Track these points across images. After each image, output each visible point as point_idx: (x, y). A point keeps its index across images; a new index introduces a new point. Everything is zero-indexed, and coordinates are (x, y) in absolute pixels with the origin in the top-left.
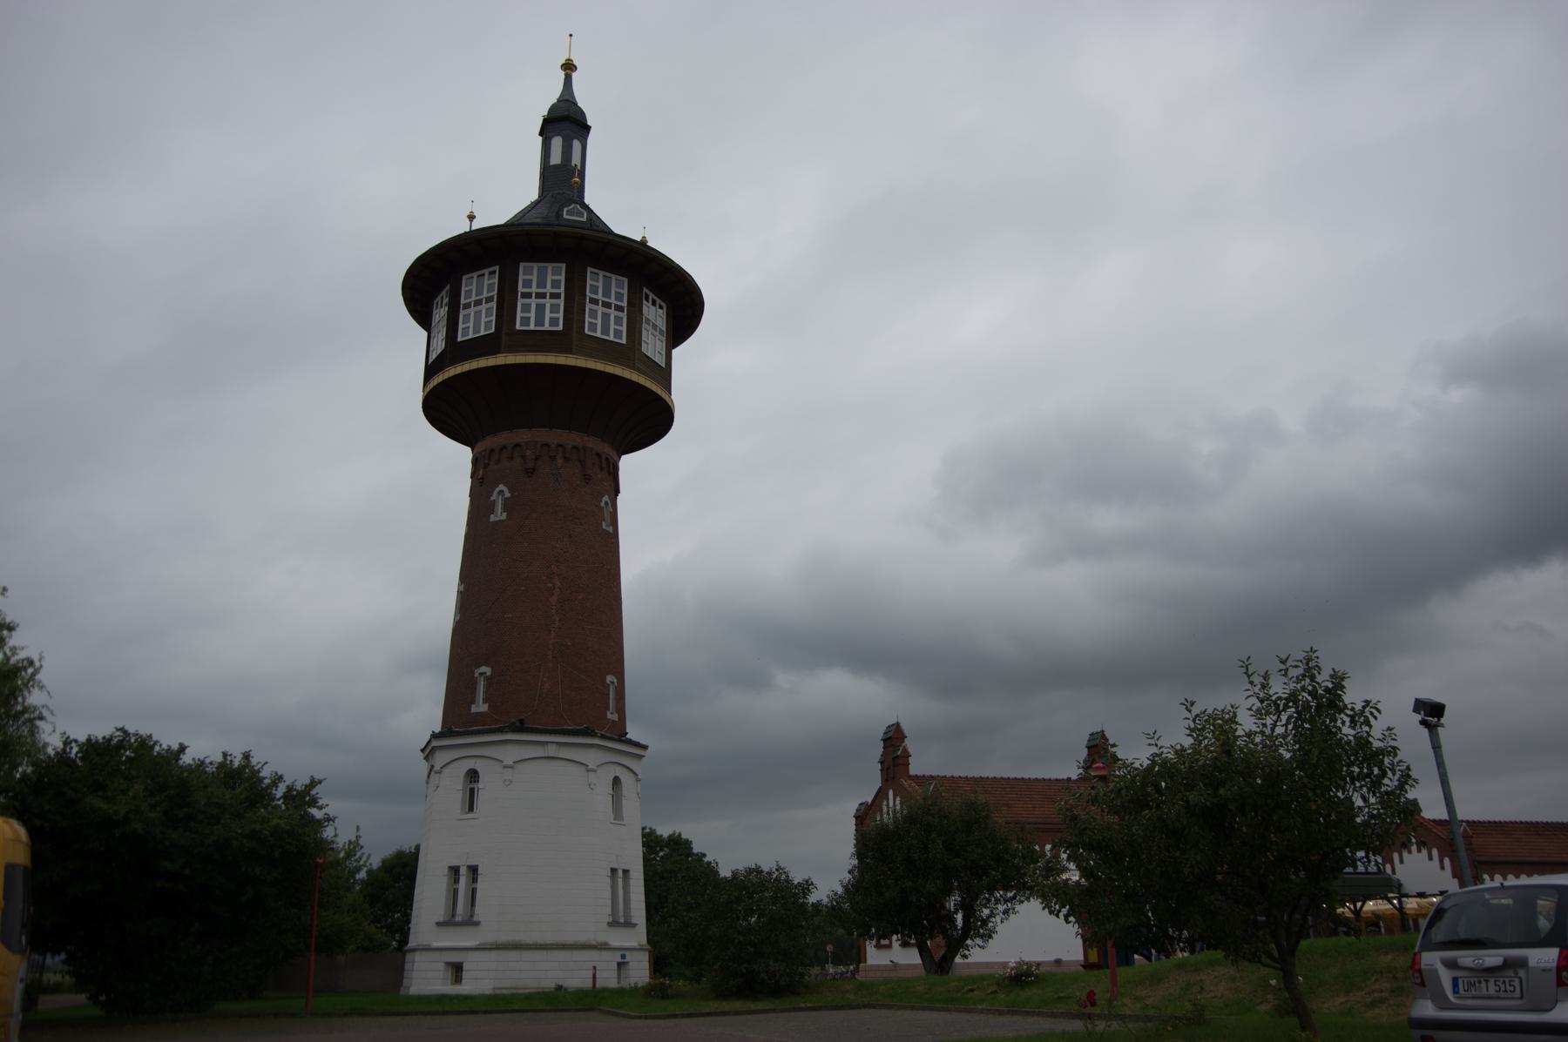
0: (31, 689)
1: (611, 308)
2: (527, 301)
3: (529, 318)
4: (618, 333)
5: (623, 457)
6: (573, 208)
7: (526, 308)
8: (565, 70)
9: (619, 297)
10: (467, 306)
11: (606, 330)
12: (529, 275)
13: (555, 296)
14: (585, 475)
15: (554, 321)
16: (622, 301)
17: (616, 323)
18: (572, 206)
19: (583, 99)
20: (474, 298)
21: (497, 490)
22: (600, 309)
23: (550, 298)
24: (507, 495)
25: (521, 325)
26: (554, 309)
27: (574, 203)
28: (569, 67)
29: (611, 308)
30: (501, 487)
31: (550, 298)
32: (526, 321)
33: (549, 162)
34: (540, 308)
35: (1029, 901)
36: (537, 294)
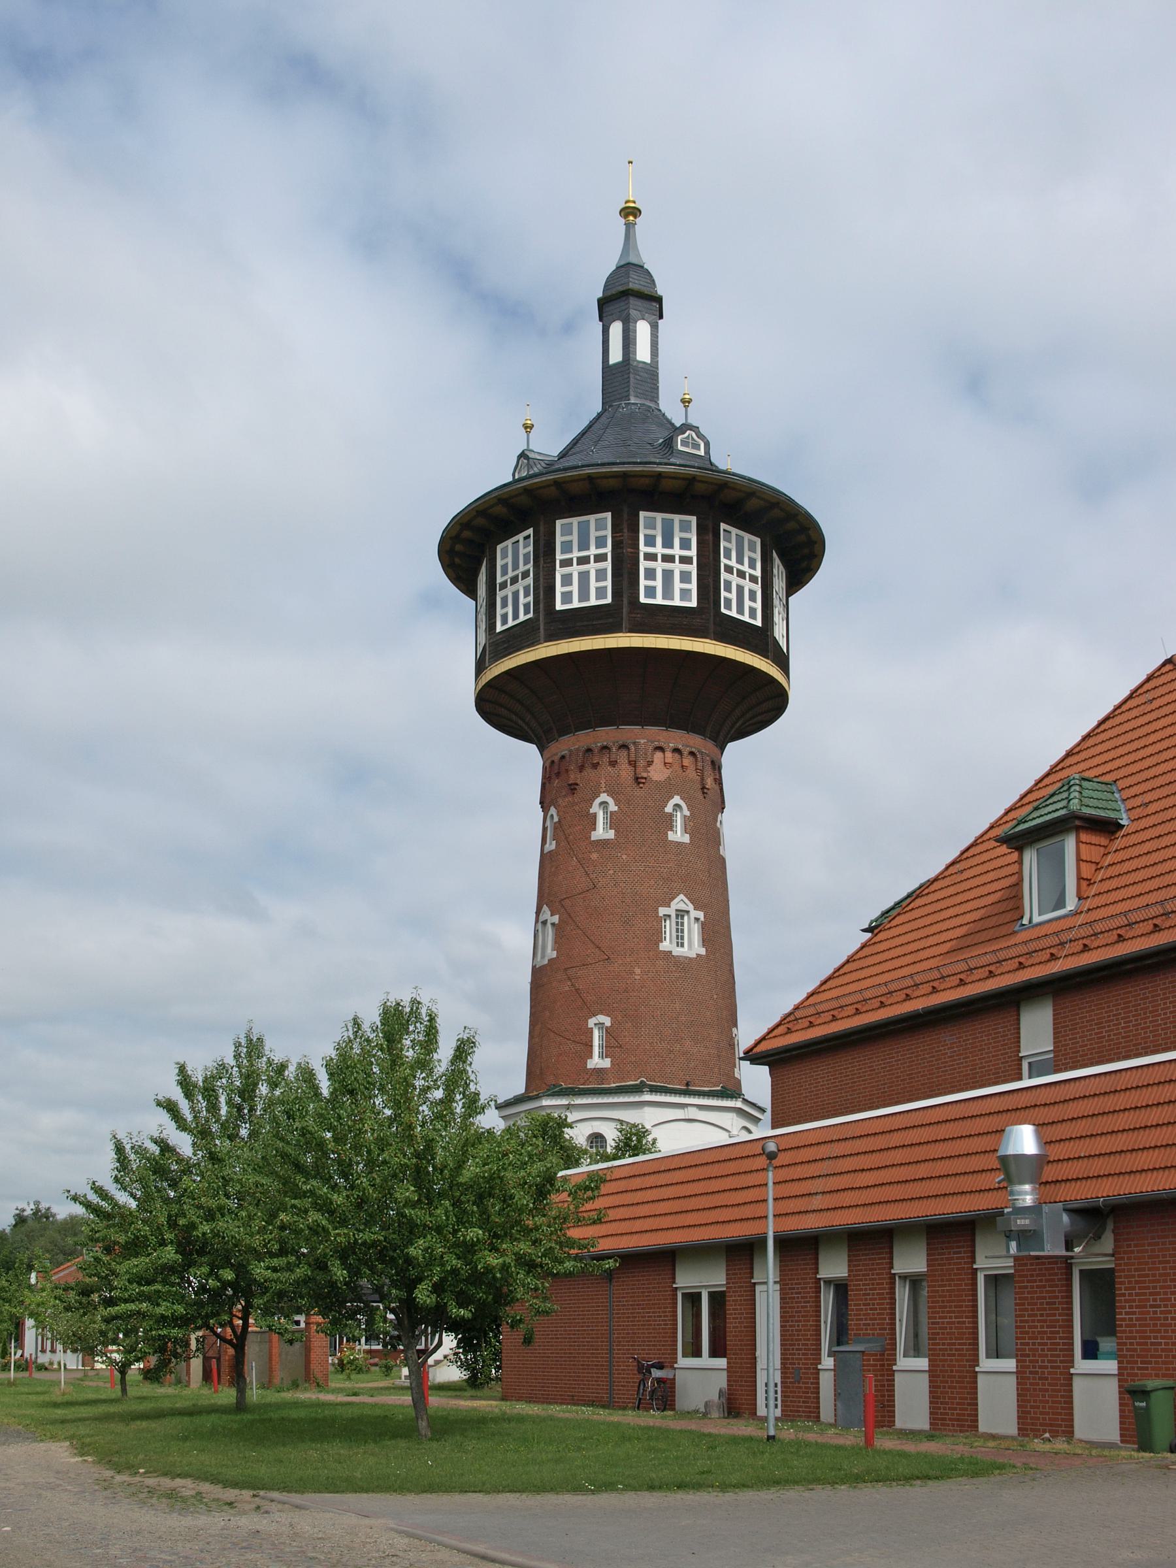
0: (243, 1042)
1: (674, 562)
2: (567, 570)
3: (571, 592)
4: (685, 594)
5: (731, 747)
6: (688, 437)
7: (567, 580)
8: (626, 216)
9: (685, 544)
10: (504, 586)
11: (668, 592)
12: (566, 530)
13: (685, 560)
14: (637, 778)
15: (601, 592)
16: (689, 549)
17: (682, 581)
18: (688, 432)
19: (650, 257)
20: (511, 574)
21: (598, 801)
22: (659, 566)
23: (663, 561)
24: (613, 807)
25: (562, 604)
26: (685, 577)
27: (691, 430)
28: (630, 212)
29: (674, 562)
30: (604, 797)
31: (663, 561)
32: (651, 591)
33: (608, 361)
34: (584, 577)
35: (706, 1405)
36: (681, 557)
